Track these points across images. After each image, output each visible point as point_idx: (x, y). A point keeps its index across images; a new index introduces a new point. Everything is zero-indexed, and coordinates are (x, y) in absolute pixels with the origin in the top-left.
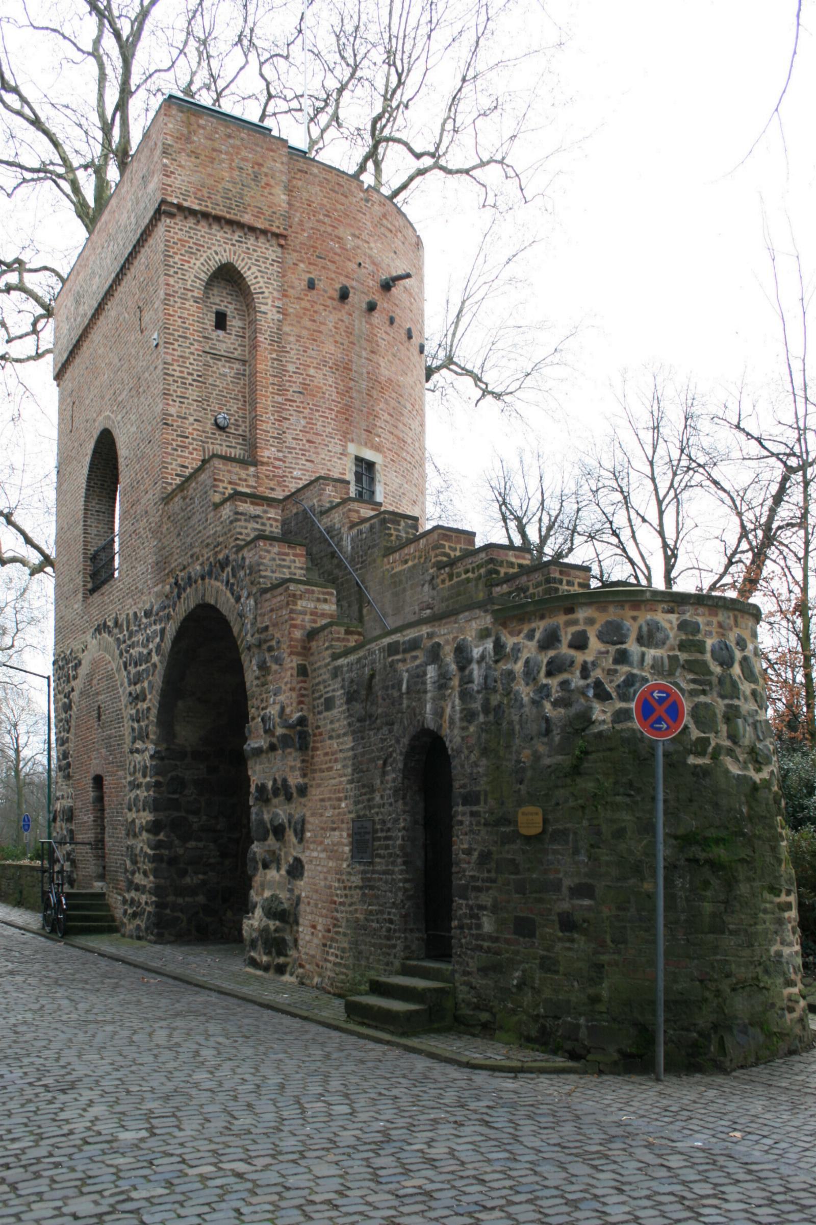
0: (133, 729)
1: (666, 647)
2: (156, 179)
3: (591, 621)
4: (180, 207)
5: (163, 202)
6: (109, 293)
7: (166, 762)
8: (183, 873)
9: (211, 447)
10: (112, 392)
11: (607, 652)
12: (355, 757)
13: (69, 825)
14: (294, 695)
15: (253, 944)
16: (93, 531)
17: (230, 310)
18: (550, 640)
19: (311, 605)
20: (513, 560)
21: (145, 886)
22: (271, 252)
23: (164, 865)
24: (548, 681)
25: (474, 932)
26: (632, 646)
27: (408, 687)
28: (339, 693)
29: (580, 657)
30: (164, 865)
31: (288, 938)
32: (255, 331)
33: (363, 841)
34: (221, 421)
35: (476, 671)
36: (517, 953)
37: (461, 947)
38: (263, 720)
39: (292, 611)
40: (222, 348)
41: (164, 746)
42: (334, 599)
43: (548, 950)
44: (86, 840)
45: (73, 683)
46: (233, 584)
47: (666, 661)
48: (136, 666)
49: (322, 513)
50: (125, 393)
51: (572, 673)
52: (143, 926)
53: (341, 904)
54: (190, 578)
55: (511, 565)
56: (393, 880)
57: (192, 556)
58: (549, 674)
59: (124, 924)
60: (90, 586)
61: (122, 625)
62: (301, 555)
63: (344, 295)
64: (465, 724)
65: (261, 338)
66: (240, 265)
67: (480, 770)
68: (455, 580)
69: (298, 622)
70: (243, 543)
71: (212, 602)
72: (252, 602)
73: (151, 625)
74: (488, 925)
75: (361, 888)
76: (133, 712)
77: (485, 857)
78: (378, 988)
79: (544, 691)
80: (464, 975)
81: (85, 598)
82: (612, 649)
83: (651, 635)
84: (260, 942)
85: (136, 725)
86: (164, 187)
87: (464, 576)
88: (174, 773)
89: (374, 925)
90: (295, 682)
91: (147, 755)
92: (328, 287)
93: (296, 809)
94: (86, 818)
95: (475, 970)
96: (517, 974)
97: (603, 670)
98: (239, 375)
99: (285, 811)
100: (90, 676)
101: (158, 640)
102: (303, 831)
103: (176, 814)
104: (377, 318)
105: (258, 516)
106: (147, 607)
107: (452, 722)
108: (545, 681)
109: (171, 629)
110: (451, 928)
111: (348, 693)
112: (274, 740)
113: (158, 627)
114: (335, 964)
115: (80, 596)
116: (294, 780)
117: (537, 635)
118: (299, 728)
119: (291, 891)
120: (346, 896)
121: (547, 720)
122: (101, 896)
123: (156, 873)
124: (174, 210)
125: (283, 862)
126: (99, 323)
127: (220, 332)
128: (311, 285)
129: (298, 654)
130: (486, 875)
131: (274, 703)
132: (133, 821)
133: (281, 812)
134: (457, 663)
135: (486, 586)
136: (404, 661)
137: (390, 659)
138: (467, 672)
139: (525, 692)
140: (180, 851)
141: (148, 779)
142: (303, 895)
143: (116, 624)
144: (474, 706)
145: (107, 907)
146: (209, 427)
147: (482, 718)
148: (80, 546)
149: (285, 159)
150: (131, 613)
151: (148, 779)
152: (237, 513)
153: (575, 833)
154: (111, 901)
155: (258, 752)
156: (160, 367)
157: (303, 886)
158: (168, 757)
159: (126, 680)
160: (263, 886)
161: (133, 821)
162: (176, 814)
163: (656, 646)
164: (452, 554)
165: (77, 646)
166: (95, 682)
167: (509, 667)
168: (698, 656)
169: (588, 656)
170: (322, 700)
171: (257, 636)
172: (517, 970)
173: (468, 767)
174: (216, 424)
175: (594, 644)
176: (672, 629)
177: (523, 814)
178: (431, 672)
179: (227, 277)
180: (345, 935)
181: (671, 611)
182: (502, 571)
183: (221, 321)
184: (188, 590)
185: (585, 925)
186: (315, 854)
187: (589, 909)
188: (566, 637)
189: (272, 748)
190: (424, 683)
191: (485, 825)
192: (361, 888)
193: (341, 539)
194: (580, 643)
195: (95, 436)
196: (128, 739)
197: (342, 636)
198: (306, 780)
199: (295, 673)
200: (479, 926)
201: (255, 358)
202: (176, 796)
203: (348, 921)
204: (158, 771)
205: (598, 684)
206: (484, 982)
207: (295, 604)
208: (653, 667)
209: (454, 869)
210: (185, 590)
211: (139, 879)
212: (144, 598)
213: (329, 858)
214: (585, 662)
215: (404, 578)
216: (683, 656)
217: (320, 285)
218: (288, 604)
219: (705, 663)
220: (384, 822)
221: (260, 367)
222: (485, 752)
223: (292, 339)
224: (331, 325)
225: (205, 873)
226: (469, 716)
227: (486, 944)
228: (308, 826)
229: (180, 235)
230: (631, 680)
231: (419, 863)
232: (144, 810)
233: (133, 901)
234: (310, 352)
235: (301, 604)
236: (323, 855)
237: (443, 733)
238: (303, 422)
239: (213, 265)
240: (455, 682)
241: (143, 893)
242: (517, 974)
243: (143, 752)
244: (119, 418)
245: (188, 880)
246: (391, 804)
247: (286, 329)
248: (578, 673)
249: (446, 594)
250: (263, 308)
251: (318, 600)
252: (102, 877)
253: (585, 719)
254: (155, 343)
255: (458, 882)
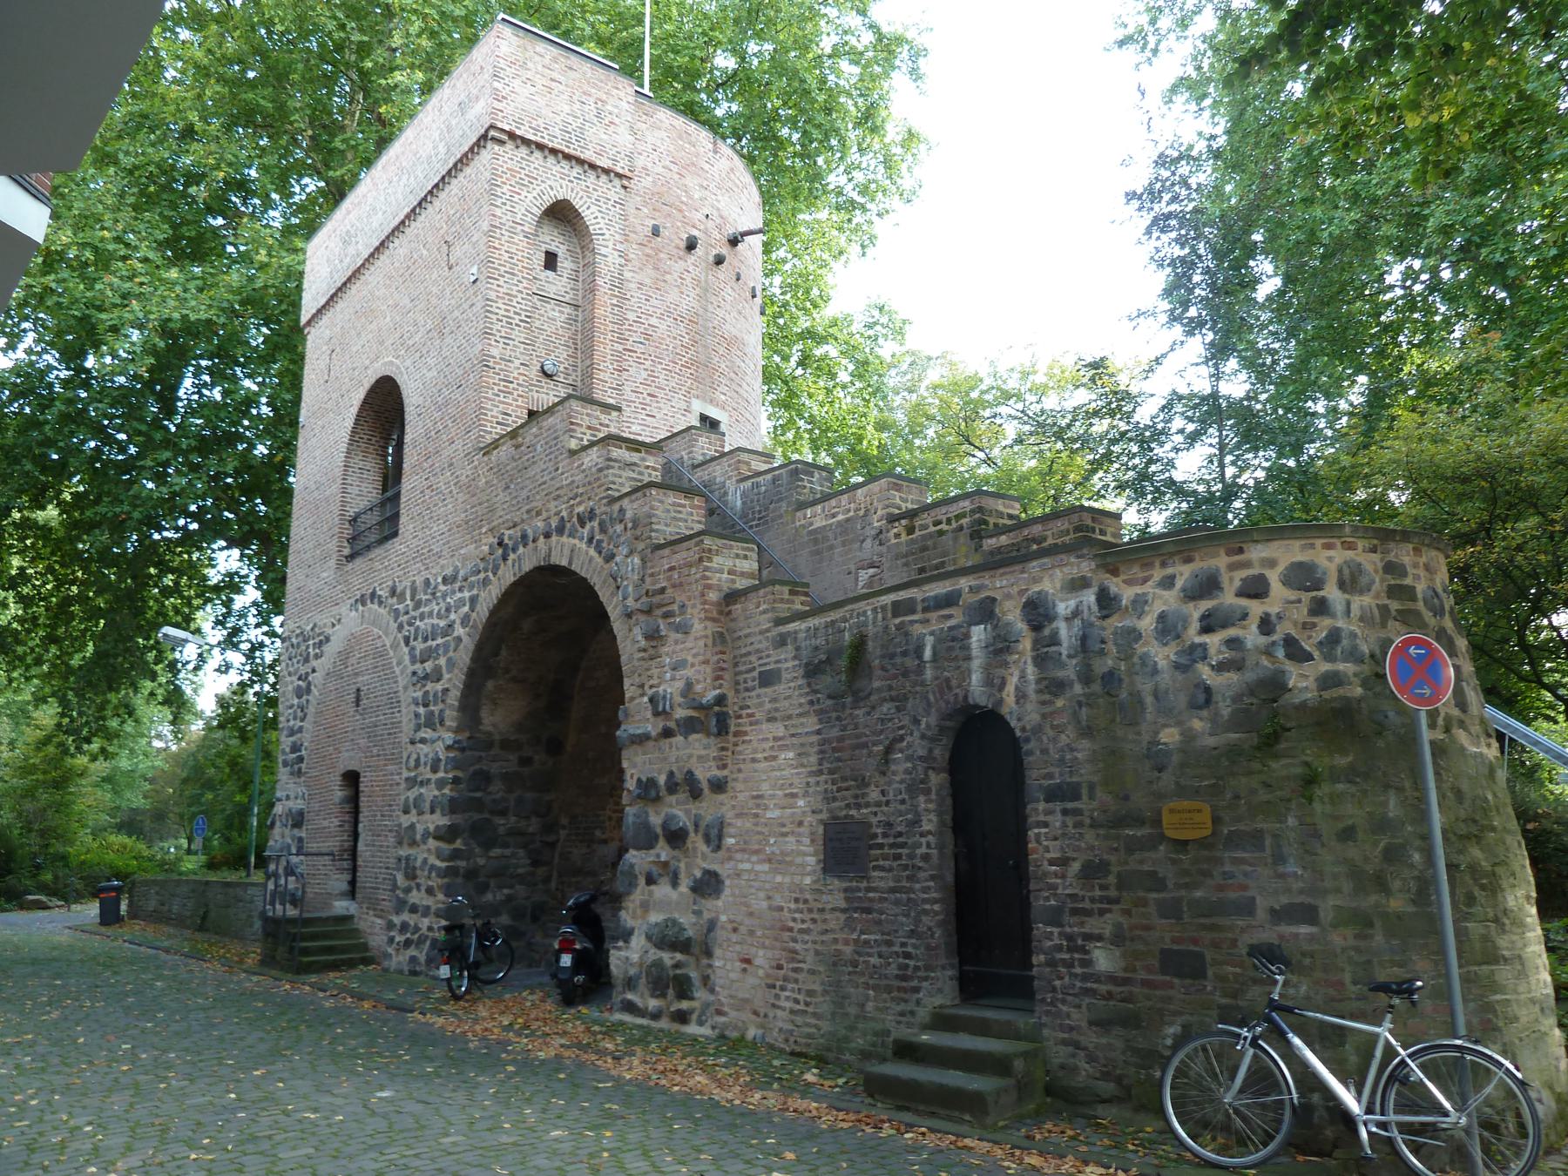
0: (417, 715)
1: (1372, 593)
2: (482, 103)
3: (1272, 563)
4: (512, 135)
5: (492, 127)
6: (399, 229)
7: (468, 753)
8: (483, 888)
9: (536, 395)
10: (397, 335)
11: (1299, 601)
12: (822, 743)
13: (296, 831)
14: (709, 670)
15: (630, 984)
16: (354, 490)
17: (561, 251)
18: (1207, 586)
19: (729, 563)
20: (1001, 508)
21: (428, 908)
22: (613, 190)
23: (459, 880)
24: (1206, 639)
25: (1078, 970)
26: (1332, 593)
27: (935, 654)
28: (790, 664)
29: (1256, 608)
30: (459, 880)
31: (693, 974)
32: (593, 274)
33: (844, 849)
34: (549, 368)
35: (1066, 634)
36: (1170, 999)
37: (1054, 990)
38: (651, 700)
39: (707, 569)
40: (551, 290)
41: (463, 736)
42: (755, 556)
43: (1235, 997)
44: (324, 850)
45: (314, 663)
46: (599, 542)
47: (1376, 611)
48: (426, 639)
49: (695, 467)
50: (420, 335)
51: (1244, 628)
52: (422, 958)
53: (801, 931)
54: (524, 536)
55: (1000, 515)
56: (909, 899)
57: (528, 512)
58: (1207, 629)
59: (388, 956)
60: (347, 552)
61: (403, 594)
62: (699, 507)
63: (691, 246)
64: (1047, 697)
65: (600, 281)
66: (577, 203)
67: (1079, 755)
68: (918, 533)
69: (714, 582)
70: (617, 494)
71: (564, 563)
72: (637, 560)
73: (453, 592)
74: (1104, 960)
75: (844, 911)
76: (419, 694)
77: (1092, 871)
78: (907, 1051)
79: (1196, 653)
80: (1063, 1030)
81: (340, 565)
82: (1306, 597)
83: (1354, 579)
84: (643, 980)
85: (421, 710)
86: (494, 112)
87: (933, 529)
88: (477, 767)
89: (874, 960)
90: (709, 655)
91: (440, 746)
92: (674, 236)
93: (709, 808)
94: (326, 823)
95: (1084, 1024)
96: (1171, 1030)
97: (1295, 624)
98: (572, 320)
99: (687, 812)
100: (345, 656)
101: (466, 609)
102: (720, 837)
103: (477, 816)
104: (724, 272)
105: (635, 464)
106: (449, 571)
107: (1021, 696)
108: (1198, 640)
109: (489, 597)
110: (1032, 966)
111: (807, 665)
112: (672, 725)
113: (467, 594)
114: (792, 1012)
115: (332, 563)
116: (703, 774)
117: (1179, 583)
118: (717, 709)
119: (698, 913)
120: (814, 921)
121: (1208, 690)
122: (347, 919)
123: (449, 891)
124: (505, 137)
125: (682, 875)
126: (378, 263)
127: (549, 273)
128: (656, 232)
129: (714, 620)
130: (1098, 893)
131: (673, 679)
132: (412, 826)
133: (680, 813)
134: (1029, 622)
135: (972, 537)
136: (926, 621)
137: (897, 621)
138: (1047, 632)
139: (1163, 655)
140: (481, 861)
141: (441, 774)
142: (723, 918)
143: (393, 592)
144: (1060, 674)
145: (355, 933)
146: (534, 372)
147: (1078, 688)
148: (335, 508)
149: (631, 99)
150: (419, 580)
151: (441, 774)
152: (610, 459)
153: (1275, 836)
154: (362, 925)
155: (642, 739)
156: (479, 305)
157: (721, 908)
158: (473, 744)
159: (407, 658)
160: (645, 906)
161: (412, 826)
162: (477, 816)
163: (1361, 592)
164: (903, 505)
165: (323, 619)
166: (352, 661)
167: (1128, 623)
168: (1409, 605)
169: (1272, 606)
170: (755, 674)
171: (644, 599)
172: (1171, 1024)
173: (1055, 747)
174: (544, 372)
175: (1277, 589)
176: (1376, 571)
177: (1172, 811)
178: (978, 634)
179: (561, 214)
180: (812, 972)
181: (1374, 550)
182: (992, 521)
183: (551, 261)
184: (521, 550)
185: (1307, 961)
186: (747, 866)
187: (1311, 938)
188: (1232, 583)
189: (667, 733)
190: (967, 648)
191: (1091, 826)
192: (844, 911)
193: (726, 493)
194: (1256, 589)
195: (367, 385)
196: (407, 726)
197: (786, 596)
198: (725, 772)
199: (710, 642)
200: (1087, 963)
201: (592, 303)
202: (478, 795)
203: (817, 953)
204: (456, 764)
205: (1290, 642)
206: (1104, 1041)
207: (710, 560)
208: (1361, 619)
209: (1032, 886)
210: (514, 550)
211: (416, 897)
212: (443, 562)
213: (776, 871)
214: (1267, 615)
215: (830, 534)
216: (1394, 606)
217: (664, 232)
218: (701, 560)
219: (1417, 614)
220: (889, 825)
221: (599, 312)
222: (1087, 732)
223: (633, 286)
224: (676, 275)
225: (511, 887)
226: (1055, 687)
227: (1103, 988)
228: (728, 830)
229: (510, 164)
230: (1334, 637)
231: (950, 878)
232: (432, 812)
233: (404, 927)
234: (654, 302)
235: (717, 561)
236: (766, 867)
237: (1004, 711)
238: (644, 374)
239: (548, 201)
240: (1026, 644)
241: (425, 915)
242: (1171, 1030)
243: (433, 742)
244: (408, 363)
245: (489, 897)
246: (903, 802)
247: (628, 275)
248: (1254, 628)
249: (904, 549)
250: (603, 251)
251: (737, 556)
252: (352, 892)
253: (1274, 686)
254: (473, 278)
255: (1042, 901)
